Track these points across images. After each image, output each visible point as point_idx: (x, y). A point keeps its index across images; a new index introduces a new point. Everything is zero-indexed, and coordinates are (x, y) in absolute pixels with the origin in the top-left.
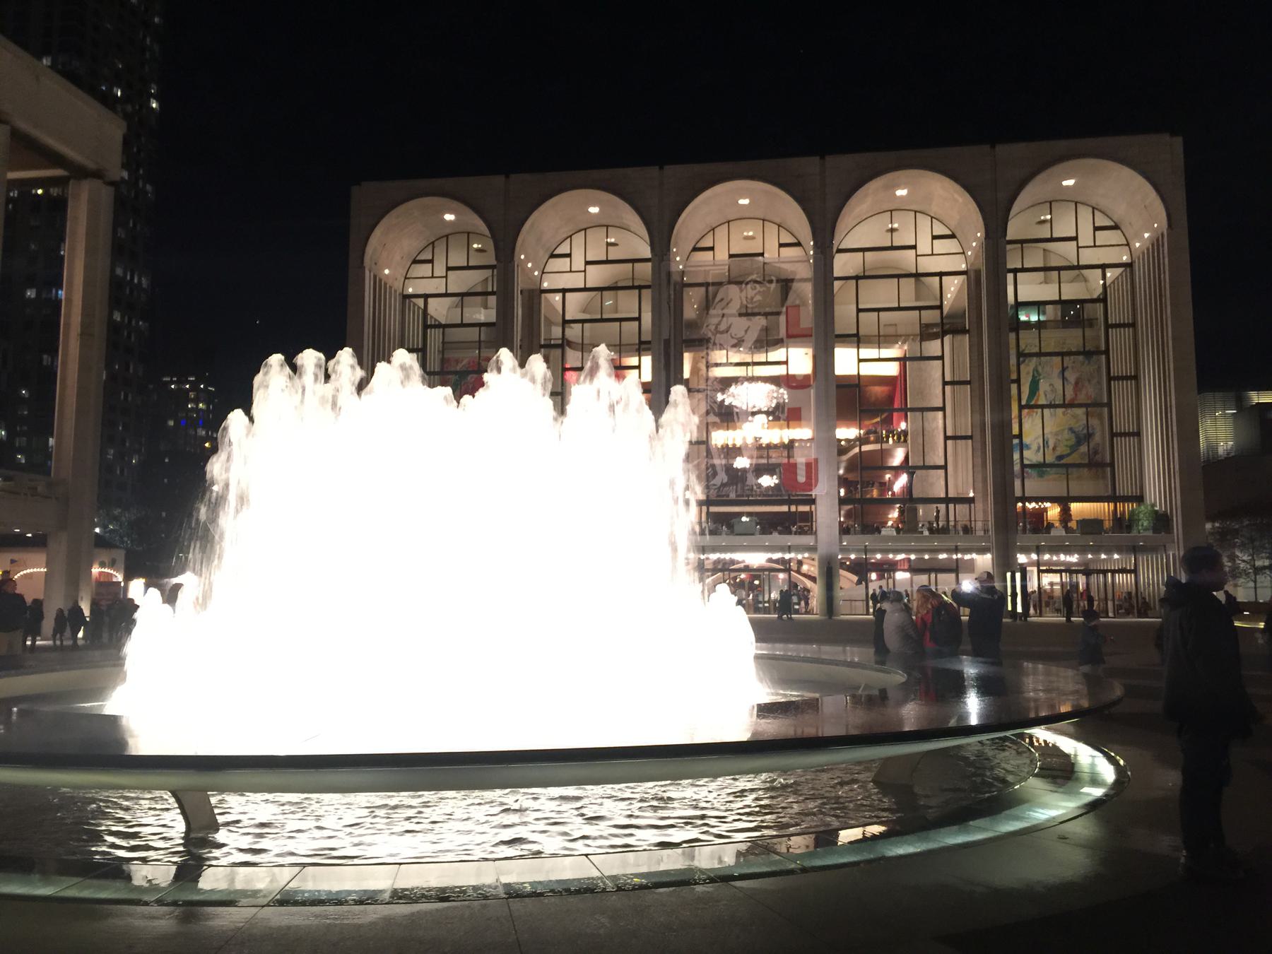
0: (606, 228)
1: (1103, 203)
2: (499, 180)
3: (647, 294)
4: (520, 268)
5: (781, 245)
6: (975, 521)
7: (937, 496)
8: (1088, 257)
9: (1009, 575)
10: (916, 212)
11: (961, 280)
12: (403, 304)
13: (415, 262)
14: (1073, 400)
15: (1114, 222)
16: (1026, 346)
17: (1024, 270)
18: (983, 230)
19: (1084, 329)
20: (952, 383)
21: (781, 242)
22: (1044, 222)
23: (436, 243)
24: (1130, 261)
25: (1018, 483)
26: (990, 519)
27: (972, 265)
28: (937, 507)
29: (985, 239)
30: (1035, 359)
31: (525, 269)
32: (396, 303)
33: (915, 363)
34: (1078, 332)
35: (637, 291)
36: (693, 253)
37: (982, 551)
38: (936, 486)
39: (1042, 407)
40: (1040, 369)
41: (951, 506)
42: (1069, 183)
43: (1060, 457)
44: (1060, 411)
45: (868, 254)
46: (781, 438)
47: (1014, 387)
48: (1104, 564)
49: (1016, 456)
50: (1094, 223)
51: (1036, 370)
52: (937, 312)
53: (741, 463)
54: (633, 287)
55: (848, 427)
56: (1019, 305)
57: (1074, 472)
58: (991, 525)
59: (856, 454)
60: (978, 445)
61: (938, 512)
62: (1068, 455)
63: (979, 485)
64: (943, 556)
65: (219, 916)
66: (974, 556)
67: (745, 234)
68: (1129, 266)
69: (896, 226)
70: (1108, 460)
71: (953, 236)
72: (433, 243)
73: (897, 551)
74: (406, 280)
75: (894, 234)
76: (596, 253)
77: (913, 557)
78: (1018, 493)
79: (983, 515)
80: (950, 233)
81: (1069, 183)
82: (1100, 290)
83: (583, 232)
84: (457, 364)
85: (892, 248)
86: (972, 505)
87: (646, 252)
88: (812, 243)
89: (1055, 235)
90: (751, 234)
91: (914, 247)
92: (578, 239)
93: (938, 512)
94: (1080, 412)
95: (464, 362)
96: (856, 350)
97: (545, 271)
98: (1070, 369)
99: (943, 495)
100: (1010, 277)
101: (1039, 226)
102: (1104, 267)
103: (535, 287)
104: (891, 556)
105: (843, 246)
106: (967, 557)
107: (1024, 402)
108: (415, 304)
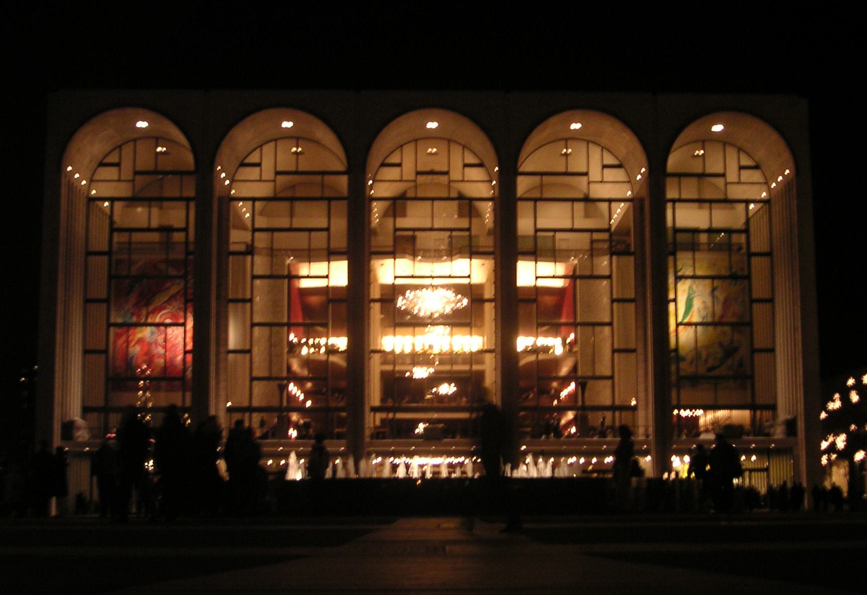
3: (192, 205)
5: (605, 166)
13: (102, 164)
14: (722, 317)
15: (619, 161)
17: (680, 200)
18: (791, 163)
20: (619, 301)
33: (586, 281)
38: (603, 395)
43: (710, 369)
46: (451, 346)
47: (672, 306)
48: (758, 464)
49: (673, 367)
53: (421, 373)
55: (527, 336)
56: (676, 231)
58: (651, 430)
60: (641, 358)
61: (604, 418)
62: (719, 366)
63: (642, 395)
68: (765, 202)
71: (619, 166)
72: (120, 146)
75: (569, 158)
76: (285, 164)
78: (674, 402)
82: (743, 220)
87: (339, 165)
89: (570, 170)
92: (268, 149)
93: (604, 418)
97: (235, 178)
100: (669, 206)
102: (747, 202)
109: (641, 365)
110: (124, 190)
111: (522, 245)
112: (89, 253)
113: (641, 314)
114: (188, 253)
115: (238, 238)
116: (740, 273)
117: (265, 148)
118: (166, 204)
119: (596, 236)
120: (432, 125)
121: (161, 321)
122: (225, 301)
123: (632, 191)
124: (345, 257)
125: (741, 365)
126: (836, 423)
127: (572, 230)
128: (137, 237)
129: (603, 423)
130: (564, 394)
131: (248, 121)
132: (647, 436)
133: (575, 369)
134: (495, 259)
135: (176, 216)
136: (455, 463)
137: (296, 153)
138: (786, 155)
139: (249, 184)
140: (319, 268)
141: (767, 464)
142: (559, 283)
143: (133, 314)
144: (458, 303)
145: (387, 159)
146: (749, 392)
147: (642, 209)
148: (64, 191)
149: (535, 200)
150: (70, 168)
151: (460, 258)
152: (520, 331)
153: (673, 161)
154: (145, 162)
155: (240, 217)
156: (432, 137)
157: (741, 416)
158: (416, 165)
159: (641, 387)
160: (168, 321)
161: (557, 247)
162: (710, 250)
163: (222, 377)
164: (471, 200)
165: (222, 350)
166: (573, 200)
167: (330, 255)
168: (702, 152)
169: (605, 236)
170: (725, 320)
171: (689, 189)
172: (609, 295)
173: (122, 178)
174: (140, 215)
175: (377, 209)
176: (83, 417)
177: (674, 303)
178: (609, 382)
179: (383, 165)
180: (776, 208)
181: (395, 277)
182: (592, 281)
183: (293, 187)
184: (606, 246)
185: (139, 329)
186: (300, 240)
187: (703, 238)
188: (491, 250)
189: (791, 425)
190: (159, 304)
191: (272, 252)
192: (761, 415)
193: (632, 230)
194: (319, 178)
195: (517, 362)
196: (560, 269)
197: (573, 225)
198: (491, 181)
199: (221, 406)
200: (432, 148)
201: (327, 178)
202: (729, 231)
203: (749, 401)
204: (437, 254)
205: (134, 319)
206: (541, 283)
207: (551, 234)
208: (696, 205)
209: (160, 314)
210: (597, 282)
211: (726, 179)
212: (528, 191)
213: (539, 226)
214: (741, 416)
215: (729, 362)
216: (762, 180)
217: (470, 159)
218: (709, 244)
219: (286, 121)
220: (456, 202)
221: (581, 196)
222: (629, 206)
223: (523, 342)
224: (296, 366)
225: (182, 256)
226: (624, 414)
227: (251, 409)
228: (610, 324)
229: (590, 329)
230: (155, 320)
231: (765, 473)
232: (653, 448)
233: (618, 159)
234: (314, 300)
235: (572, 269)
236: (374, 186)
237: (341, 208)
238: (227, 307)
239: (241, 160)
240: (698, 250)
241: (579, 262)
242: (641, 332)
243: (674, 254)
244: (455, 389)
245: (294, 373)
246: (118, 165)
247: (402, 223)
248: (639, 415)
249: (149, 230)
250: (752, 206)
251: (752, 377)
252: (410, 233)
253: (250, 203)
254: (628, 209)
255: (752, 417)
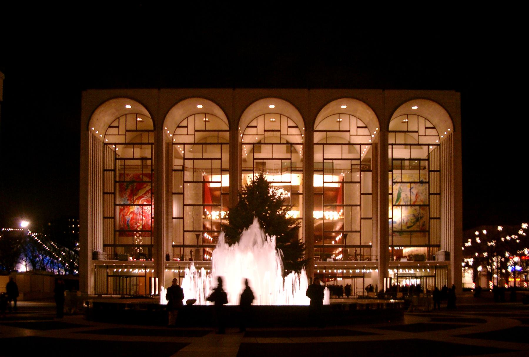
0: (338, 115)
1: (429, 117)
2: (154, 91)
4: (165, 134)
5: (358, 127)
6: (372, 255)
7: (355, 244)
8: (423, 140)
9: (385, 279)
10: (418, 116)
11: (369, 147)
12: (104, 147)
13: (110, 127)
14: (415, 202)
16: (396, 177)
17: (395, 144)
19: (420, 170)
21: (358, 126)
22: (405, 122)
23: (120, 118)
24: (439, 143)
25: (390, 238)
26: (378, 255)
27: (374, 140)
28: (356, 249)
29: (380, 131)
30: (399, 184)
31: (167, 134)
32: (100, 148)
34: (417, 172)
35: (220, 145)
36: (177, 128)
37: (374, 268)
38: (354, 239)
39: (402, 206)
40: (402, 188)
41: (362, 249)
42: (415, 108)
43: (408, 227)
44: (409, 207)
45: (328, 133)
47: (390, 196)
50: (425, 125)
51: (400, 188)
52: (359, 161)
54: (218, 144)
56: (393, 159)
57: (415, 234)
58: (378, 257)
59: (321, 223)
60: (375, 222)
61: (356, 251)
63: (374, 240)
64: (358, 271)
65: (300, 274)
66: (371, 270)
67: (271, 120)
69: (341, 120)
70: (427, 229)
72: (119, 118)
73: (338, 268)
74: (106, 136)
76: (200, 126)
77: (345, 271)
78: (390, 244)
79: (376, 252)
80: (433, 126)
81: (415, 108)
83: (194, 116)
84: (128, 176)
85: (339, 131)
86: (446, 250)
88: (304, 128)
90: (274, 120)
91: (417, 132)
92: (191, 119)
93: (356, 251)
94: (417, 207)
95: (131, 176)
96: (322, 175)
97: (175, 134)
98: (414, 188)
99: (358, 244)
100: (390, 147)
101: (403, 124)
102: (429, 145)
103: (170, 142)
104: (335, 271)
105: (316, 129)
106: (368, 271)
107: (394, 204)
108: (108, 147)
109: (375, 225)
110: (122, 139)
111: (315, 167)
112: (105, 170)
113: (375, 200)
114: (152, 170)
115: (177, 163)
116: (424, 181)
117: (190, 118)
118: (144, 146)
119: (354, 162)
120: (272, 107)
121: (142, 203)
122: (170, 194)
123: (372, 141)
124: (228, 172)
125: (423, 225)
126: (469, 252)
127: (342, 159)
128: (128, 162)
129: (356, 253)
130: (337, 239)
131: (179, 105)
132: (377, 260)
133: (343, 227)
134: (303, 173)
135: (148, 152)
136: (291, 272)
137: (206, 121)
138: (449, 122)
139: (183, 136)
140: (216, 178)
141: (435, 272)
142: (337, 185)
143: (128, 200)
144: (286, 195)
145: (180, 124)
146: (427, 238)
147: (376, 148)
148: (90, 140)
149: (323, 144)
150: (93, 129)
151: (287, 173)
152: (315, 208)
153: (392, 125)
154: (131, 126)
155: (178, 152)
156: (271, 113)
157: (422, 250)
158: (264, 128)
159: (374, 236)
160: (145, 203)
161: (335, 168)
162: (410, 169)
163: (170, 230)
164: (292, 144)
165: (170, 217)
166: (342, 144)
167: (222, 171)
168: (407, 120)
169: (358, 162)
170: (416, 204)
171: (400, 139)
172: (360, 192)
173: (120, 134)
174: (130, 152)
175: (246, 150)
176: (104, 250)
177: (391, 195)
178: (359, 234)
179: (248, 127)
180: (443, 148)
181: (324, 182)
182: (351, 184)
183: (206, 138)
184: (359, 167)
185: (131, 207)
186: (207, 164)
187: (407, 163)
188: (302, 169)
189: (447, 255)
190: (141, 195)
191: (194, 170)
192: (433, 250)
193: (371, 160)
194: (216, 133)
195: (313, 223)
196: (336, 178)
197: (342, 157)
198: (301, 135)
199: (170, 244)
200: (273, 119)
201: (220, 133)
202: (419, 160)
203: (427, 243)
204: (275, 171)
205: (129, 202)
206: (326, 185)
207: (331, 161)
208: (404, 146)
209: (141, 200)
210: (354, 184)
211: (350, 133)
212: (322, 140)
213: (255, 157)
214: (422, 250)
215: (418, 224)
216: (437, 134)
217: (291, 124)
218: (409, 166)
219: (271, 105)
220: (285, 146)
221: (347, 142)
222: (370, 147)
223: (317, 214)
224: (208, 225)
225: (150, 172)
226: (366, 249)
227: (184, 246)
228: (360, 205)
229: (350, 207)
230: (139, 202)
231: (434, 278)
232: (379, 266)
233: (364, 123)
234: (218, 193)
235: (342, 178)
236: (243, 137)
237: (226, 148)
238: (172, 197)
239: (178, 125)
240: (404, 169)
241: (345, 175)
242: (375, 209)
243: (392, 171)
244: (509, 239)
245: (208, 228)
246: (118, 127)
247: (257, 156)
248: (373, 250)
249: (133, 159)
250: (114, 146)
251: (429, 231)
252: (262, 161)
253: (183, 146)
254: (369, 149)
255: (428, 251)
